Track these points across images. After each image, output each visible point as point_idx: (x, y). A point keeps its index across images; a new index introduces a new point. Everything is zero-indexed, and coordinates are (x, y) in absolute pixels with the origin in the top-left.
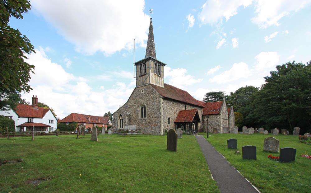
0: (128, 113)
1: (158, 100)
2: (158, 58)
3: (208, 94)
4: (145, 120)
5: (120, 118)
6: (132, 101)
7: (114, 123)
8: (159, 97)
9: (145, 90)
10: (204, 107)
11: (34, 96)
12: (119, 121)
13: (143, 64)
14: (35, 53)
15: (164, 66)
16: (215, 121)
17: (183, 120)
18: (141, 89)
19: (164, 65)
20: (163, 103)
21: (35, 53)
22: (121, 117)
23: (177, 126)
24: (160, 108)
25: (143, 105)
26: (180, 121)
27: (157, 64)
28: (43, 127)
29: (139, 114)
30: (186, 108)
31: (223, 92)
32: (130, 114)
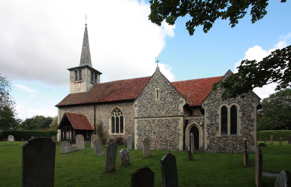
2: (95, 66)
13: (79, 71)
14: (229, 24)
15: (100, 74)
19: (100, 73)
21: (229, 24)
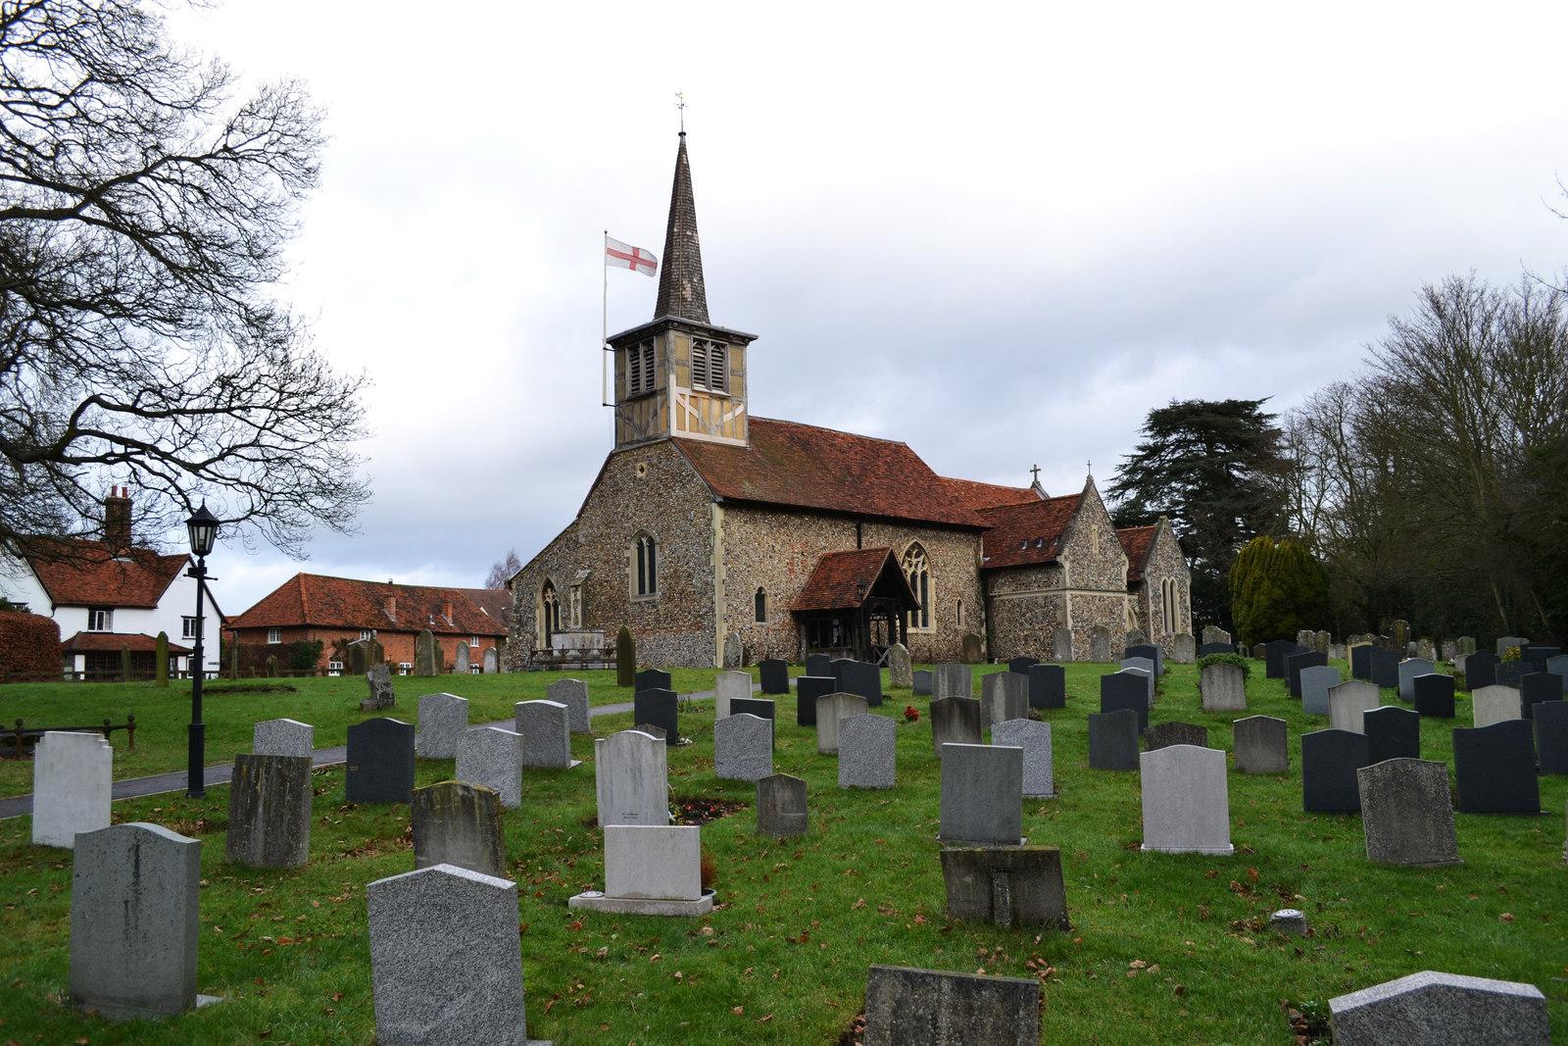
0: (582, 574)
1: (705, 513)
2: (719, 317)
3: (1162, 421)
4: (654, 607)
5: (544, 598)
6: (596, 516)
7: (520, 621)
8: (708, 498)
9: (651, 465)
10: (990, 529)
11: (114, 488)
12: (540, 613)
13: (644, 344)
15: (30, 755)
16: (1041, 601)
17: (827, 599)
18: (636, 460)
19: (744, 340)
20: (725, 525)
22: (550, 593)
23: (803, 628)
24: (712, 548)
25: (645, 534)
26: (814, 607)
27: (706, 342)
28: (150, 656)
29: (627, 575)
30: (864, 540)
31: (1254, 405)
32: (587, 579)
